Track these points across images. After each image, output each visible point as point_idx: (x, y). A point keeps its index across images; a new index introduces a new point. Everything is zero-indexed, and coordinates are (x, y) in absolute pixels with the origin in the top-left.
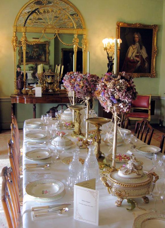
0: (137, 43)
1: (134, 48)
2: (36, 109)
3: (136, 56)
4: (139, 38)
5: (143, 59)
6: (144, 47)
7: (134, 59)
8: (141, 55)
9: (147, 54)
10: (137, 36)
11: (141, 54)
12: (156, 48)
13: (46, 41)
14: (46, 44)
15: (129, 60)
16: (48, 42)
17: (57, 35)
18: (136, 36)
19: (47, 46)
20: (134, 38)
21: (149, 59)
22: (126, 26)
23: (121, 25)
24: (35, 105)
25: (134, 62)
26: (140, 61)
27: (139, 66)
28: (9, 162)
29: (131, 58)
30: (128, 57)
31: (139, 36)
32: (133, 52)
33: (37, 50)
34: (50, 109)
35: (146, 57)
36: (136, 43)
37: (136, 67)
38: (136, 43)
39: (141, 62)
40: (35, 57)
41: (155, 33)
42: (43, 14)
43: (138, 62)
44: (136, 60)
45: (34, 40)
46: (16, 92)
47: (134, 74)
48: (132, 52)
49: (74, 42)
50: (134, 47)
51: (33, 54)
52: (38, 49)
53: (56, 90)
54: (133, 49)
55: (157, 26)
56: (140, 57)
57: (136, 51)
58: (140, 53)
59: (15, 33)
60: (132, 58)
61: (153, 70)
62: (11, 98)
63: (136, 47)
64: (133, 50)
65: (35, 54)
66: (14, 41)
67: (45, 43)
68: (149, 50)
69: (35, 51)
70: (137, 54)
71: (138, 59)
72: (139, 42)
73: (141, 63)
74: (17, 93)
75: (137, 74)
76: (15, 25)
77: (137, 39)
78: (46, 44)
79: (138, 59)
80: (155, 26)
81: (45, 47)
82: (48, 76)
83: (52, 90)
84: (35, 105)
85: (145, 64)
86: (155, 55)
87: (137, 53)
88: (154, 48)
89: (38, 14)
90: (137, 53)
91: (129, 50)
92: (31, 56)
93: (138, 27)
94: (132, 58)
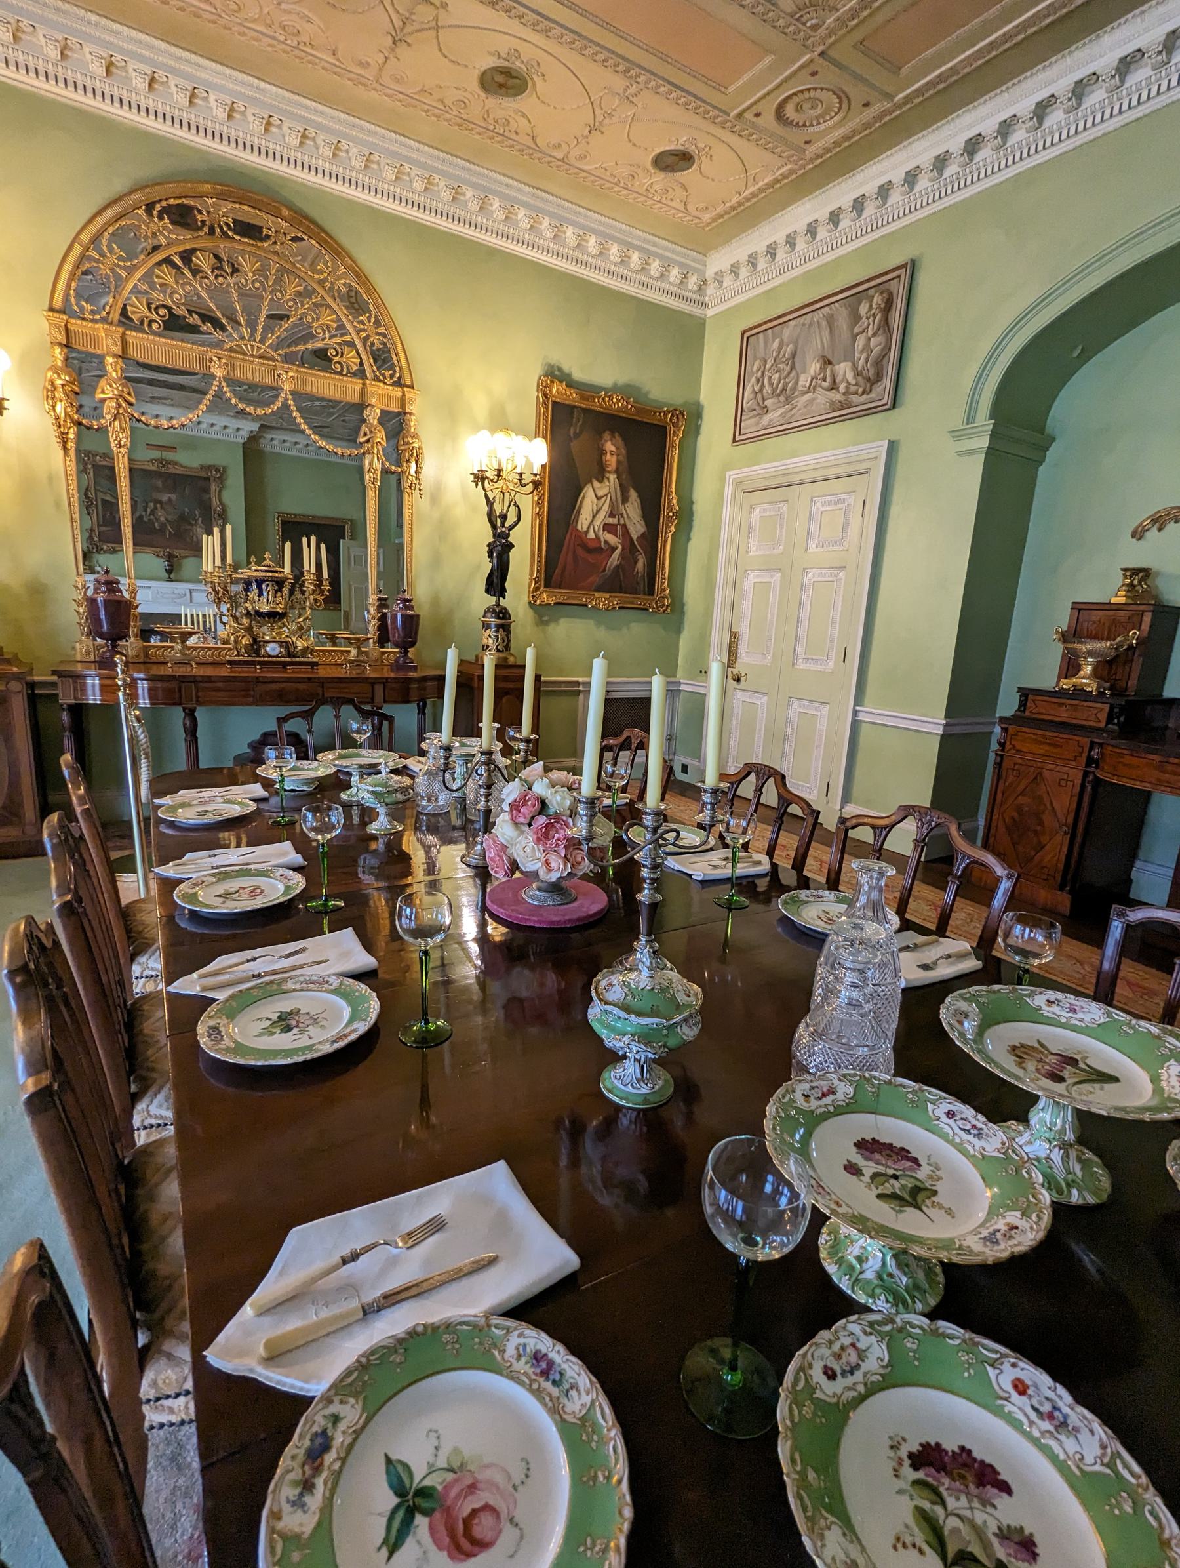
0: (612, 477)
1: (600, 494)
2: (199, 734)
3: (607, 527)
4: (621, 458)
5: (631, 539)
6: (633, 494)
7: (598, 538)
8: (625, 525)
9: (643, 522)
10: (613, 448)
11: (622, 522)
12: (674, 501)
13: (210, 467)
14: (208, 479)
15: (581, 538)
16: (217, 470)
17: (286, 400)
18: (609, 446)
19: (214, 487)
20: (602, 452)
21: (651, 539)
22: (573, 400)
23: (554, 390)
24: (193, 711)
25: (600, 550)
26: (620, 547)
27: (617, 567)
28: (1068, 903)
29: (587, 532)
30: (579, 527)
31: (617, 448)
32: (598, 511)
33: (170, 499)
34: (511, 546)
35: (640, 534)
36: (608, 475)
37: (604, 570)
38: (608, 475)
39: (623, 549)
40: (163, 526)
41: (675, 442)
42: (212, 278)
43: (614, 549)
44: (606, 542)
45: (156, 454)
46: (88, 653)
47: (597, 595)
48: (594, 509)
49: (368, 441)
50: (603, 489)
51: (152, 513)
52: (173, 497)
53: (300, 644)
54: (598, 498)
55: (682, 413)
56: (620, 531)
57: (606, 507)
58: (622, 515)
59: (58, 350)
60: (591, 535)
61: (664, 587)
62: (55, 678)
63: (606, 491)
64: (595, 500)
65: (162, 515)
66: (59, 394)
67: (203, 474)
68: (652, 511)
69: (160, 502)
70: (613, 521)
71: (612, 539)
72: (617, 471)
73: (622, 556)
74: (92, 658)
75: (607, 596)
76: (58, 302)
77: (611, 461)
78: (208, 479)
79: (612, 539)
80: (677, 414)
81: (207, 491)
82: (260, 582)
83: (281, 646)
84: (190, 714)
85: (636, 562)
86: (673, 528)
87: (612, 515)
88: (670, 501)
89: (187, 272)
90: (612, 515)
91: (581, 503)
92: (145, 519)
93: (619, 410)
94: (591, 535)
